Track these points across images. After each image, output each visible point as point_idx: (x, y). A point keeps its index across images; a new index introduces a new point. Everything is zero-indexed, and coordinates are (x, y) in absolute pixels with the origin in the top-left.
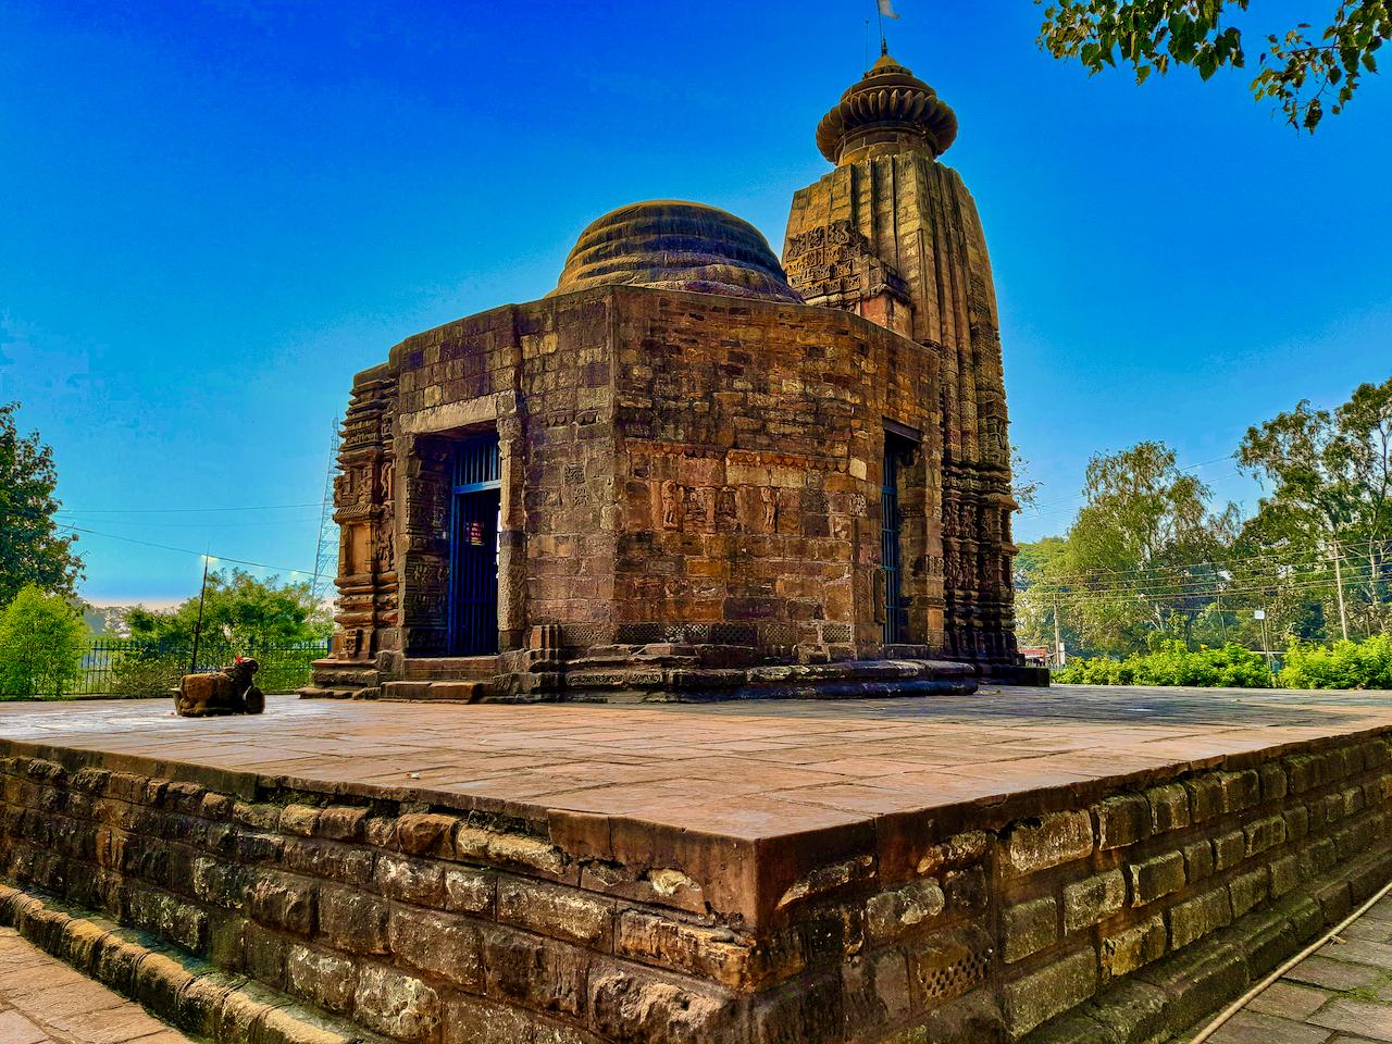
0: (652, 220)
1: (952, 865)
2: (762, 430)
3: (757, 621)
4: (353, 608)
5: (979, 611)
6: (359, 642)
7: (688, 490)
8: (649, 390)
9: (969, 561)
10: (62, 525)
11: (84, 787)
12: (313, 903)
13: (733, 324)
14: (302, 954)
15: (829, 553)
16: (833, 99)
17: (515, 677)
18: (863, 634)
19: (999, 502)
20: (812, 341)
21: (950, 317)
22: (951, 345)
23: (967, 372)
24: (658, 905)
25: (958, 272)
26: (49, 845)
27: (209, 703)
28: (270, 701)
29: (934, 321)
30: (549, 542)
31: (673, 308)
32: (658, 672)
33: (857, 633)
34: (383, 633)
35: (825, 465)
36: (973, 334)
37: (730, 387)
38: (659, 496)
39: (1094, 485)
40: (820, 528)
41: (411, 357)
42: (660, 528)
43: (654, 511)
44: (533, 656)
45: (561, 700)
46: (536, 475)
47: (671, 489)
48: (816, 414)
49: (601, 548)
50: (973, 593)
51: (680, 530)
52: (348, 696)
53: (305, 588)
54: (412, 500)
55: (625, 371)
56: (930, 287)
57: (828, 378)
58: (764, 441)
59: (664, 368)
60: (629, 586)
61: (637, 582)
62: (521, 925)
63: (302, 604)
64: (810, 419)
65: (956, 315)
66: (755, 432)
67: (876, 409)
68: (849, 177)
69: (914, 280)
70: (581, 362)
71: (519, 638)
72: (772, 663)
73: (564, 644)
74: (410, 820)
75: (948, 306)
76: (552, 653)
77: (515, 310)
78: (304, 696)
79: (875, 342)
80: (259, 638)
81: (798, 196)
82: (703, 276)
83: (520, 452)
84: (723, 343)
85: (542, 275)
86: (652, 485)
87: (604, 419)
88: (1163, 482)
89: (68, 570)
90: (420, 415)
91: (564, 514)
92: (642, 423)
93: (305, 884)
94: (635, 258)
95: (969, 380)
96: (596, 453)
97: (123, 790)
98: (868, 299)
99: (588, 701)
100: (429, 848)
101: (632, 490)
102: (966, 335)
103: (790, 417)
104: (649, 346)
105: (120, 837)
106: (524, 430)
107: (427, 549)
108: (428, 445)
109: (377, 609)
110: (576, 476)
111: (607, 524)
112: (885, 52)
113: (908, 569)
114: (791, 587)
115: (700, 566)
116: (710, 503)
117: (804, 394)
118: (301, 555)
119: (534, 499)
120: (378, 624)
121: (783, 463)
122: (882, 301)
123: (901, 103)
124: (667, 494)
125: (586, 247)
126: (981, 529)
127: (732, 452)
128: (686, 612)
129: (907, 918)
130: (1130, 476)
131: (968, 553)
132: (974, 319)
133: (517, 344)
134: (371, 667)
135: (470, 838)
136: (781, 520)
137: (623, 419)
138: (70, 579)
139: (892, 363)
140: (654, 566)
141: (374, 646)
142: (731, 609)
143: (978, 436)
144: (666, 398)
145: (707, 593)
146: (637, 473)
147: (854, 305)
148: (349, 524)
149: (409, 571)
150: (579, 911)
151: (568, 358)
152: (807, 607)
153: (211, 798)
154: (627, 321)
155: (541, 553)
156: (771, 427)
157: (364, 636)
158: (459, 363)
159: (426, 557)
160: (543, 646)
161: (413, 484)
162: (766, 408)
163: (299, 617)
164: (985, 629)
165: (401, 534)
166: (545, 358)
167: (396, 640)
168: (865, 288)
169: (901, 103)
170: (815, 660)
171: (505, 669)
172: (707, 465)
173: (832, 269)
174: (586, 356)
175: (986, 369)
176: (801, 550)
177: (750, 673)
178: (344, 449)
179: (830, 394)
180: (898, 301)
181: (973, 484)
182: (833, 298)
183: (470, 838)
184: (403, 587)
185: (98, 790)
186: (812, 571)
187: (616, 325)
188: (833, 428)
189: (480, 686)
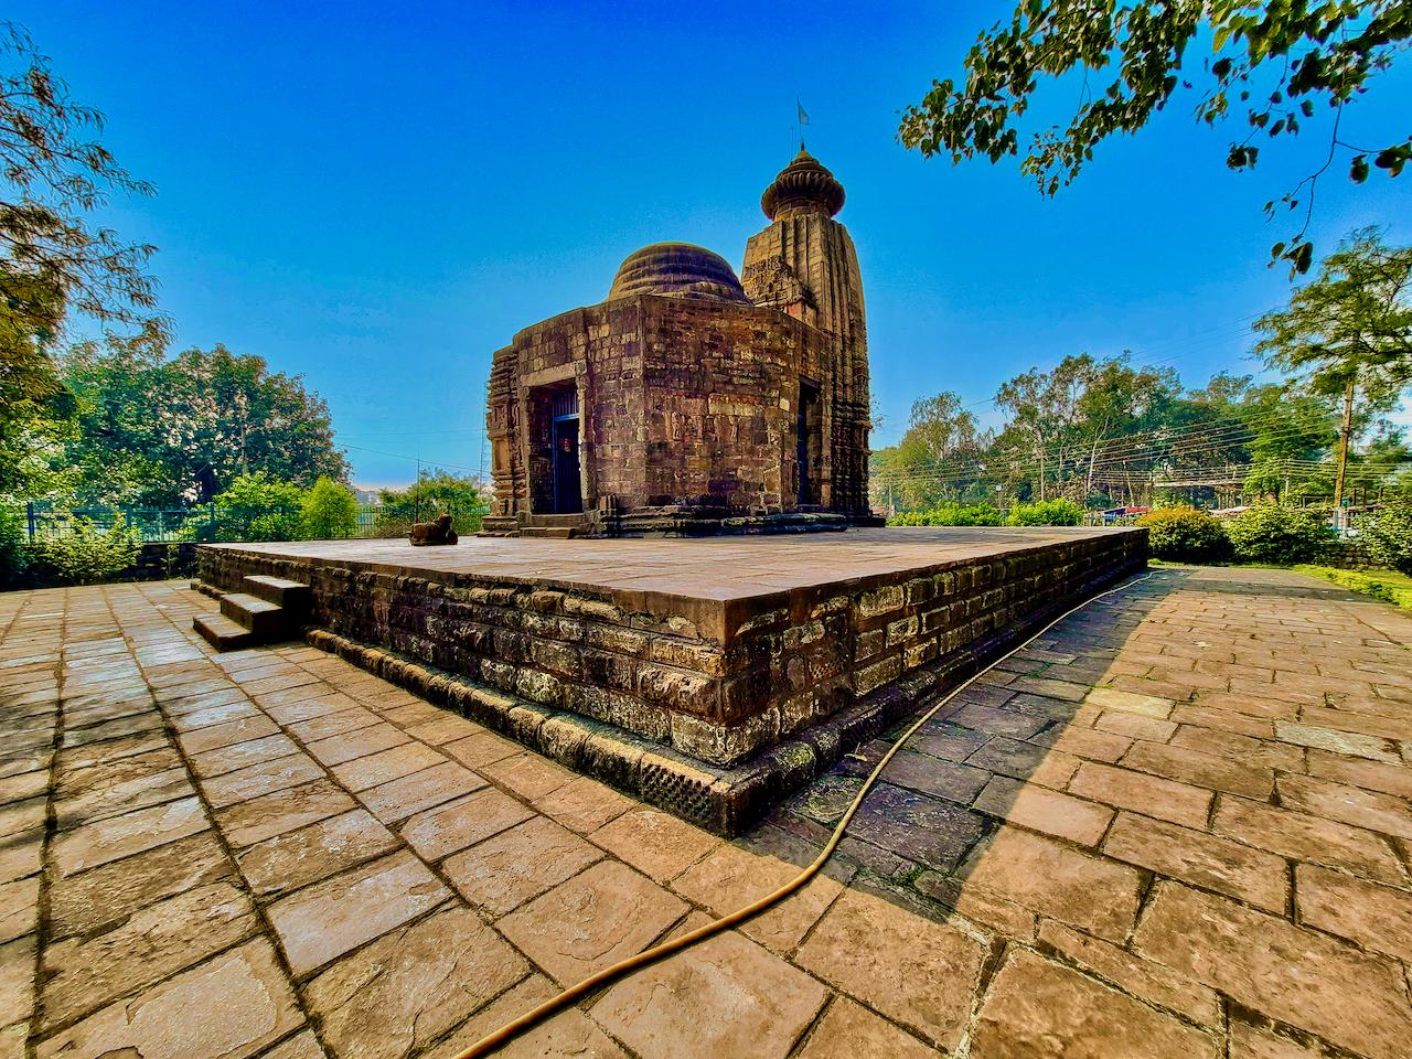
0: (663, 255)
2: (730, 382)
4: (502, 487)
6: (507, 506)
7: (687, 418)
8: (663, 359)
11: (364, 582)
12: (489, 638)
14: (488, 663)
15: (768, 453)
21: (838, 316)
22: (838, 332)
27: (427, 539)
32: (671, 521)
33: (783, 498)
36: (851, 326)
38: (670, 422)
40: (763, 440)
41: (525, 341)
46: (599, 409)
49: (637, 453)
53: (475, 478)
54: (530, 425)
55: (649, 347)
57: (768, 351)
58: (730, 388)
59: (671, 345)
62: (600, 646)
65: (842, 315)
66: (725, 383)
70: (623, 342)
71: (593, 504)
73: (619, 506)
74: (538, 595)
75: (837, 309)
76: (612, 512)
77: (584, 311)
78: (479, 536)
86: (666, 414)
87: (637, 376)
88: (952, 415)
89: (344, 469)
93: (486, 628)
94: (654, 278)
95: (848, 353)
96: (632, 397)
97: (385, 582)
98: (791, 304)
100: (550, 609)
104: (663, 332)
105: (386, 607)
106: (592, 381)
108: (537, 393)
109: (515, 488)
111: (640, 438)
112: (803, 147)
113: (811, 462)
117: (754, 360)
118: (470, 456)
119: (598, 424)
120: (516, 496)
124: (675, 420)
128: (687, 488)
129: (805, 640)
135: (571, 603)
137: (648, 375)
141: (515, 509)
142: (713, 486)
143: (852, 387)
145: (698, 475)
146: (657, 407)
148: (497, 440)
153: (431, 585)
157: (510, 504)
158: (552, 344)
162: (732, 369)
163: (473, 495)
164: (853, 496)
165: (526, 448)
166: (602, 340)
167: (527, 504)
169: (812, 180)
172: (699, 402)
173: (771, 286)
174: (626, 338)
176: (752, 452)
177: (722, 521)
183: (571, 603)
184: (528, 475)
185: (372, 582)
187: (644, 319)
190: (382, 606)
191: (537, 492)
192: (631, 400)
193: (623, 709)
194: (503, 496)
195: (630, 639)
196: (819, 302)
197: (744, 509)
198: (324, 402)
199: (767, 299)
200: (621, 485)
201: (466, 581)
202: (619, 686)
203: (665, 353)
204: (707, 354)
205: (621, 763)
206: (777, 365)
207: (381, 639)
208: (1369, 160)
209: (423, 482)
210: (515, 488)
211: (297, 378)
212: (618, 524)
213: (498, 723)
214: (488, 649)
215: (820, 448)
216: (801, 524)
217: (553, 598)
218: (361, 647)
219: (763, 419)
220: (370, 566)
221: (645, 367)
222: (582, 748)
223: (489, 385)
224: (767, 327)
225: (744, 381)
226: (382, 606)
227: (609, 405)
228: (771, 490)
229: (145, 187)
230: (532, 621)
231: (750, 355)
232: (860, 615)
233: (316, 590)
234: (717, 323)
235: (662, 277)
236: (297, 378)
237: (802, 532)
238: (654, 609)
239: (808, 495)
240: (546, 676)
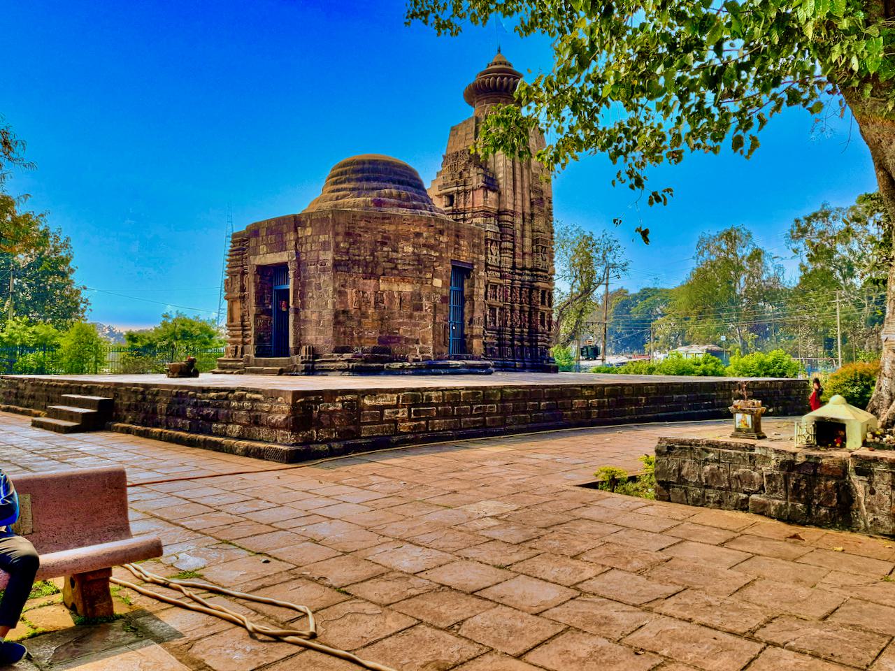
0: (360, 167)
1: (347, 400)
2: (396, 268)
3: (392, 345)
4: (233, 336)
6: (236, 351)
7: (364, 293)
8: (347, 253)
9: (524, 315)
10: (77, 279)
11: (152, 394)
12: (216, 414)
13: (383, 224)
14: (215, 425)
15: (423, 318)
16: (472, 79)
17: (295, 366)
18: (437, 350)
19: (539, 287)
20: (418, 230)
21: (519, 196)
22: (519, 210)
23: (526, 223)
24: (279, 403)
25: (525, 172)
26: (141, 411)
27: (179, 373)
28: (201, 375)
29: (510, 200)
30: (309, 312)
31: (358, 218)
32: (346, 364)
33: (434, 349)
34: (246, 347)
35: (421, 281)
36: (532, 204)
37: (382, 250)
38: (351, 294)
39: (701, 253)
40: (419, 308)
41: (254, 231)
42: (352, 308)
43: (349, 301)
44: (302, 358)
45: (313, 375)
46: (304, 285)
47: (356, 292)
48: (418, 261)
49: (328, 316)
51: (360, 309)
52: (232, 373)
53: (213, 322)
54: (256, 293)
55: (337, 245)
56: (508, 182)
57: (424, 245)
58: (396, 272)
59: (354, 243)
60: (339, 331)
61: (342, 330)
62: (257, 410)
63: (214, 329)
64: (416, 263)
65: (523, 195)
66: (392, 269)
67: (448, 258)
68: (474, 123)
69: (501, 178)
70: (320, 240)
71: (297, 352)
72: (397, 361)
73: (314, 353)
74: (237, 393)
75: (519, 190)
76: (309, 357)
77: (295, 216)
78: (214, 373)
79: (448, 228)
80: (191, 347)
81: (453, 129)
82: (379, 195)
83: (297, 275)
84: (379, 232)
85: (306, 195)
86: (348, 291)
87: (329, 264)
88: (745, 250)
89: (82, 306)
90: (258, 257)
91: (314, 301)
92: (345, 265)
93: (215, 410)
94: (351, 185)
95: (528, 227)
96: (326, 278)
97: (164, 393)
98: (476, 190)
100: (241, 399)
101: (340, 293)
102: (527, 204)
103: (407, 262)
104: (348, 234)
105: (165, 406)
106: (299, 266)
107: (263, 313)
108: (262, 270)
109: (244, 337)
110: (319, 287)
111: (330, 306)
112: (499, 51)
113: (467, 322)
114: (406, 331)
115: (367, 322)
116: (373, 298)
117: (413, 253)
118: (211, 308)
119: (303, 295)
120: (244, 343)
121: (404, 281)
122: (481, 191)
123: (501, 84)
124: (354, 294)
125: (333, 177)
126: (531, 299)
127: (382, 277)
128: (362, 341)
129: (330, 409)
130: (724, 247)
131: (524, 311)
132: (532, 196)
133: (296, 231)
134: (241, 361)
135: (248, 395)
136: (402, 304)
137: (336, 264)
138: (83, 311)
139: (457, 236)
140: (349, 323)
141: (243, 353)
142: (380, 341)
143: (531, 255)
144: (354, 255)
145: (371, 335)
146: (342, 286)
148: (232, 301)
149: (255, 322)
150: (266, 406)
151: (316, 238)
152: (412, 340)
153: (190, 393)
154: (338, 224)
155: (306, 317)
156: (399, 266)
157: (239, 351)
158: (273, 236)
159: (262, 316)
161: (256, 285)
162: (397, 259)
163: (210, 337)
164: (531, 347)
165: (252, 308)
166: (307, 237)
167: (251, 350)
168: (474, 184)
169: (501, 84)
170: (415, 360)
171: (292, 362)
172: (372, 282)
173: (461, 174)
174: (322, 238)
175: (540, 223)
176: (411, 317)
177: (385, 365)
178: (230, 261)
179: (425, 252)
180: (491, 190)
181: (527, 278)
182: (460, 188)
183: (248, 395)
184: (253, 329)
185: (157, 394)
186: (415, 325)
187: (334, 226)
188: (425, 267)
190: (162, 406)
191: (259, 340)
192: (324, 281)
193: (264, 433)
194: (234, 343)
195: (266, 406)
196: (501, 186)
197: (404, 357)
198: (68, 239)
199: (457, 184)
200: (317, 339)
201: (208, 390)
202: (262, 425)
203: (349, 249)
204: (379, 248)
205: (259, 449)
206: (431, 255)
207: (160, 424)
208: (647, 193)
209: (165, 325)
210: (244, 337)
211: (42, 215)
212: (313, 366)
213: (217, 447)
214: (216, 419)
215: (473, 312)
216: (446, 368)
217: (240, 395)
218: (148, 428)
219: (419, 294)
220: (156, 386)
221: (334, 259)
222: (247, 447)
223: (228, 258)
224: (423, 229)
225: (406, 267)
226: (162, 406)
227: (310, 283)
228: (424, 343)
229: (31, 165)
230: (234, 404)
231: (410, 249)
232: (364, 403)
233: (118, 401)
234: (387, 227)
235: (358, 185)
236: (42, 215)
237: (445, 374)
238: (273, 395)
239: (462, 347)
240: (238, 426)
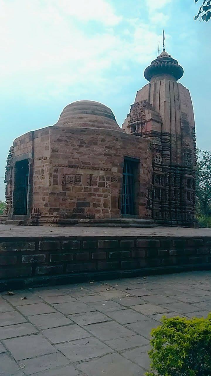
5: (180, 207)
50: (178, 202)
95: (179, 142)
98: (148, 122)
99: (91, 226)
147: (144, 123)
160: (34, 213)
189: (21, 222)
